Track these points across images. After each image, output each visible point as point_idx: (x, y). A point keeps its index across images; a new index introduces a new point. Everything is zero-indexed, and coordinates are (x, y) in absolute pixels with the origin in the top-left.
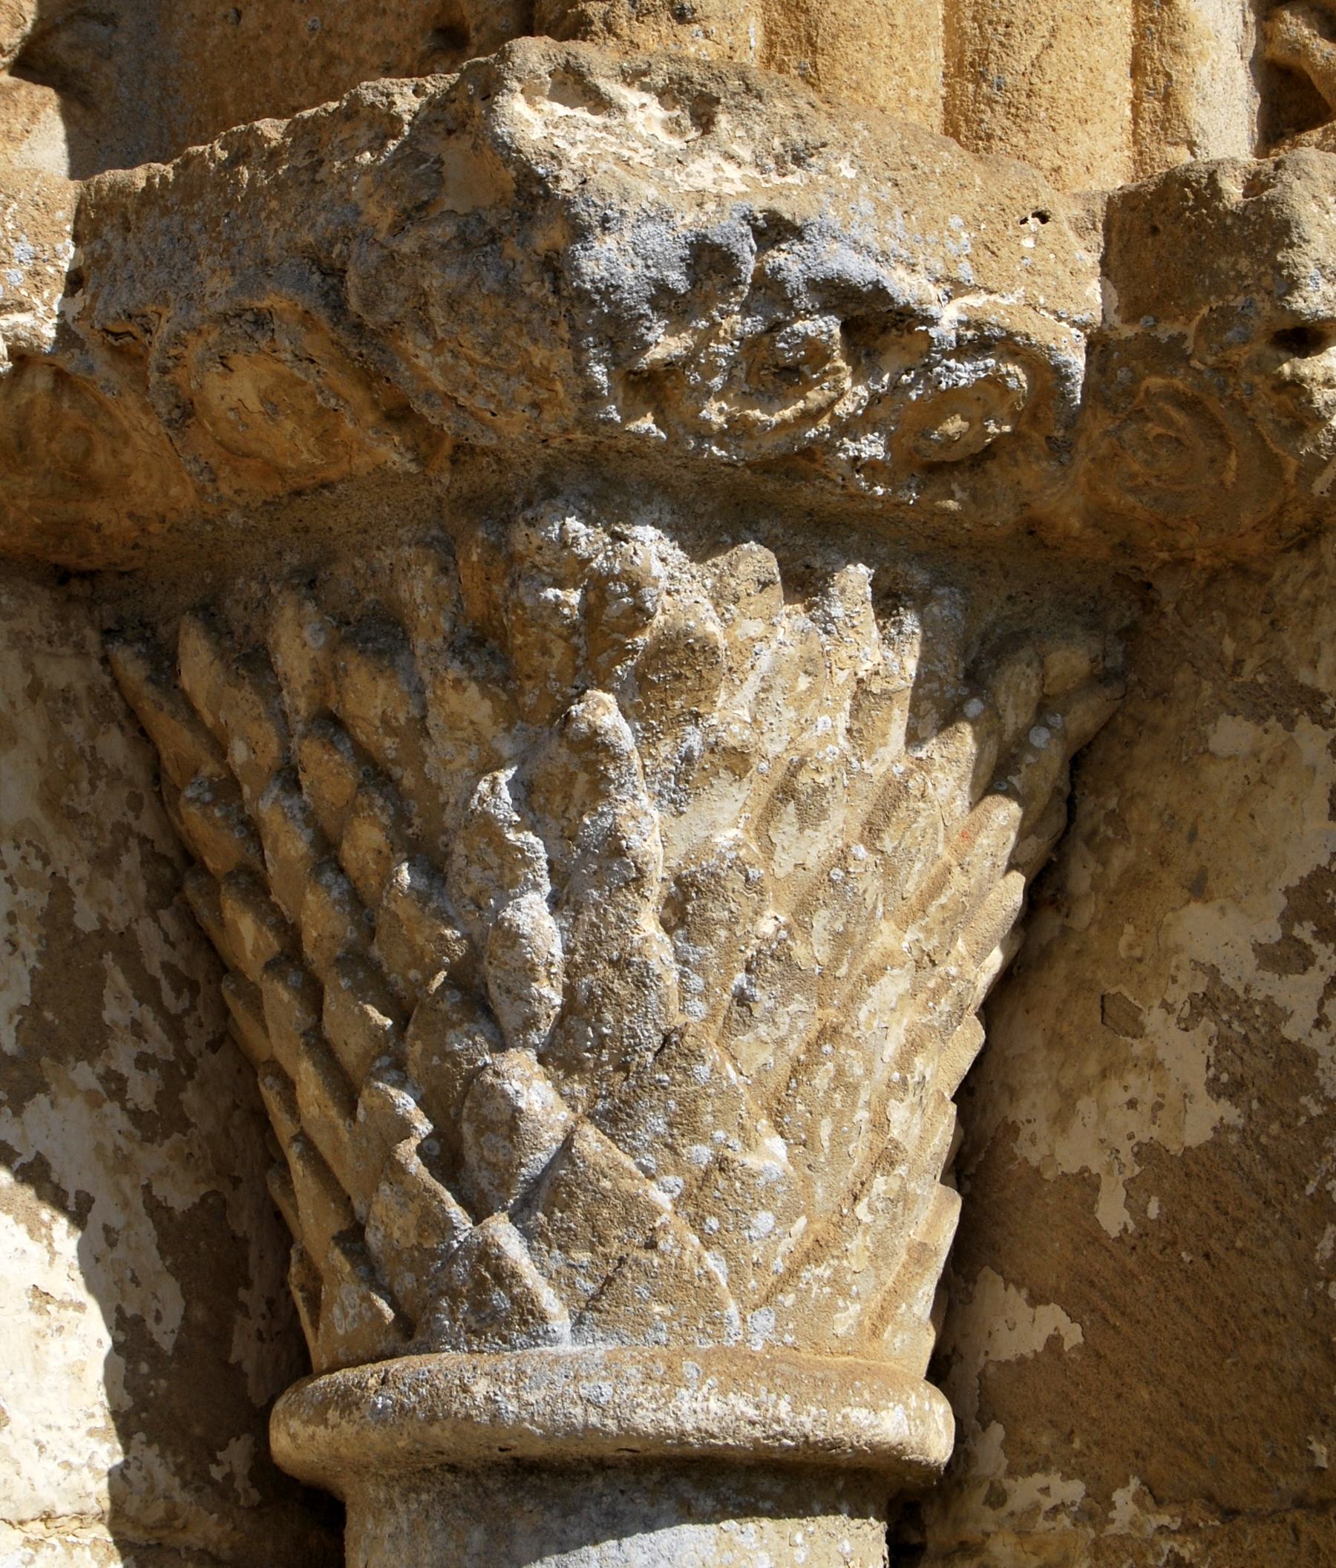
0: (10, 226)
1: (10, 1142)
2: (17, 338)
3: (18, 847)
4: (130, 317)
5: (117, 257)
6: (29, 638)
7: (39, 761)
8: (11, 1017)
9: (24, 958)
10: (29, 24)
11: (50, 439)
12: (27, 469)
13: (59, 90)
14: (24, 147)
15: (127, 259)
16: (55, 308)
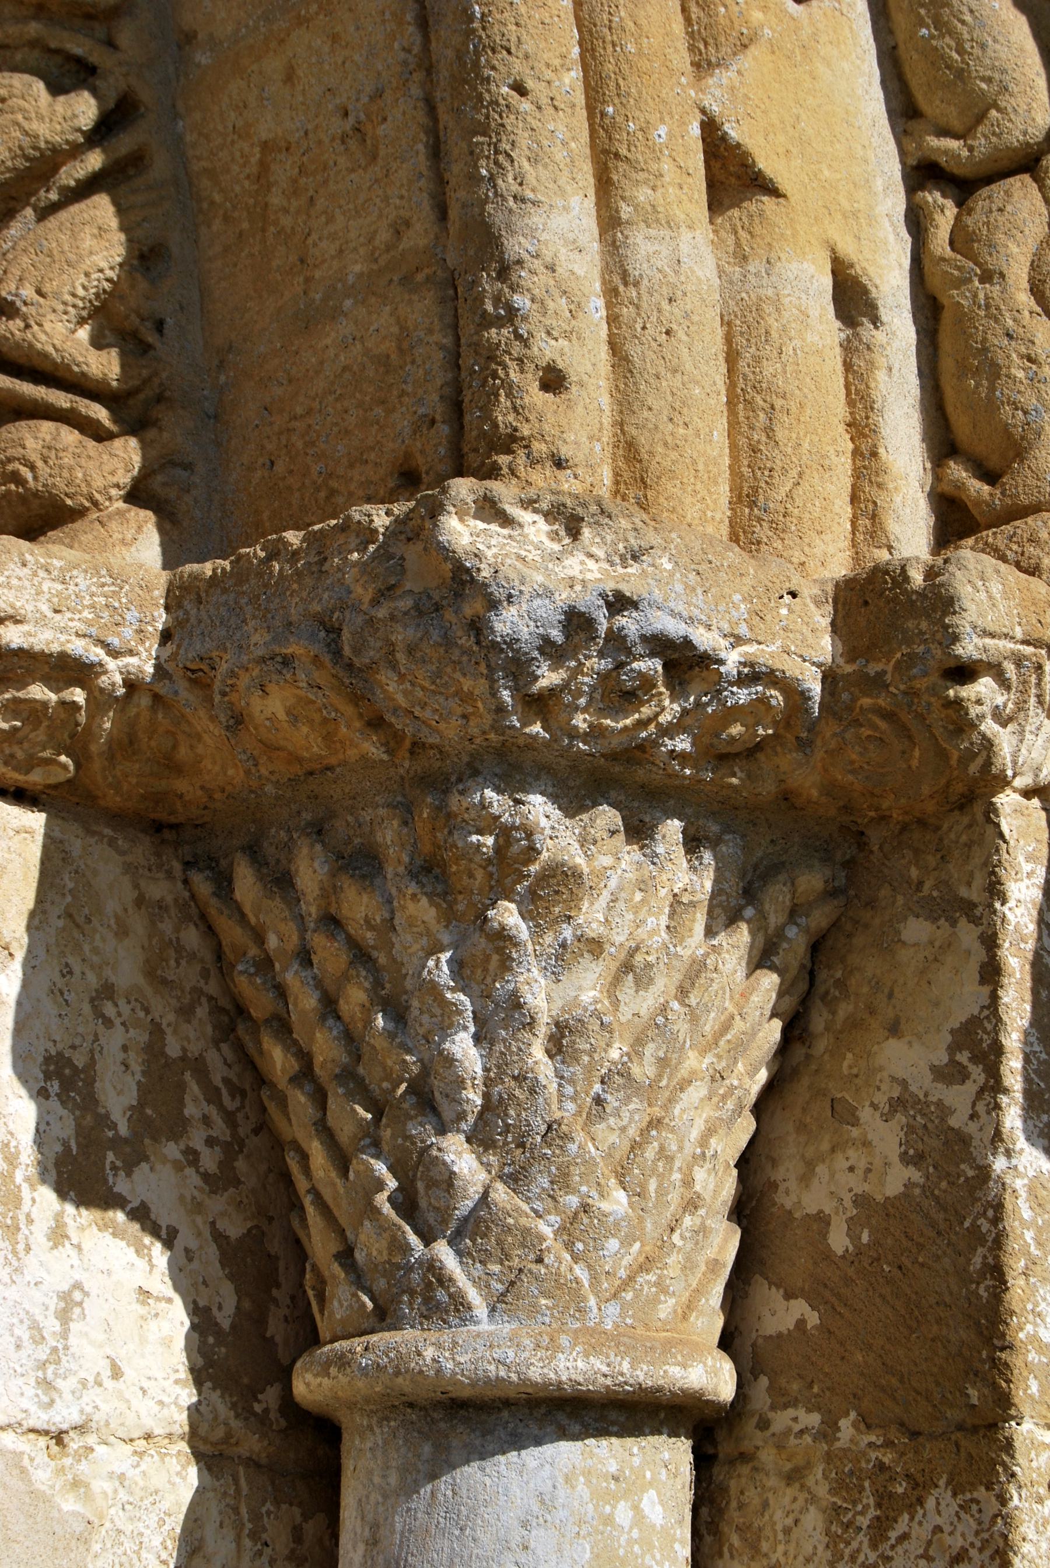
0: (124, 600)
2: (129, 673)
3: (129, 1002)
5: (193, 620)
7: (143, 947)
11: (150, 739)
13: (155, 512)
14: (133, 549)
15: (200, 622)
16: (154, 653)
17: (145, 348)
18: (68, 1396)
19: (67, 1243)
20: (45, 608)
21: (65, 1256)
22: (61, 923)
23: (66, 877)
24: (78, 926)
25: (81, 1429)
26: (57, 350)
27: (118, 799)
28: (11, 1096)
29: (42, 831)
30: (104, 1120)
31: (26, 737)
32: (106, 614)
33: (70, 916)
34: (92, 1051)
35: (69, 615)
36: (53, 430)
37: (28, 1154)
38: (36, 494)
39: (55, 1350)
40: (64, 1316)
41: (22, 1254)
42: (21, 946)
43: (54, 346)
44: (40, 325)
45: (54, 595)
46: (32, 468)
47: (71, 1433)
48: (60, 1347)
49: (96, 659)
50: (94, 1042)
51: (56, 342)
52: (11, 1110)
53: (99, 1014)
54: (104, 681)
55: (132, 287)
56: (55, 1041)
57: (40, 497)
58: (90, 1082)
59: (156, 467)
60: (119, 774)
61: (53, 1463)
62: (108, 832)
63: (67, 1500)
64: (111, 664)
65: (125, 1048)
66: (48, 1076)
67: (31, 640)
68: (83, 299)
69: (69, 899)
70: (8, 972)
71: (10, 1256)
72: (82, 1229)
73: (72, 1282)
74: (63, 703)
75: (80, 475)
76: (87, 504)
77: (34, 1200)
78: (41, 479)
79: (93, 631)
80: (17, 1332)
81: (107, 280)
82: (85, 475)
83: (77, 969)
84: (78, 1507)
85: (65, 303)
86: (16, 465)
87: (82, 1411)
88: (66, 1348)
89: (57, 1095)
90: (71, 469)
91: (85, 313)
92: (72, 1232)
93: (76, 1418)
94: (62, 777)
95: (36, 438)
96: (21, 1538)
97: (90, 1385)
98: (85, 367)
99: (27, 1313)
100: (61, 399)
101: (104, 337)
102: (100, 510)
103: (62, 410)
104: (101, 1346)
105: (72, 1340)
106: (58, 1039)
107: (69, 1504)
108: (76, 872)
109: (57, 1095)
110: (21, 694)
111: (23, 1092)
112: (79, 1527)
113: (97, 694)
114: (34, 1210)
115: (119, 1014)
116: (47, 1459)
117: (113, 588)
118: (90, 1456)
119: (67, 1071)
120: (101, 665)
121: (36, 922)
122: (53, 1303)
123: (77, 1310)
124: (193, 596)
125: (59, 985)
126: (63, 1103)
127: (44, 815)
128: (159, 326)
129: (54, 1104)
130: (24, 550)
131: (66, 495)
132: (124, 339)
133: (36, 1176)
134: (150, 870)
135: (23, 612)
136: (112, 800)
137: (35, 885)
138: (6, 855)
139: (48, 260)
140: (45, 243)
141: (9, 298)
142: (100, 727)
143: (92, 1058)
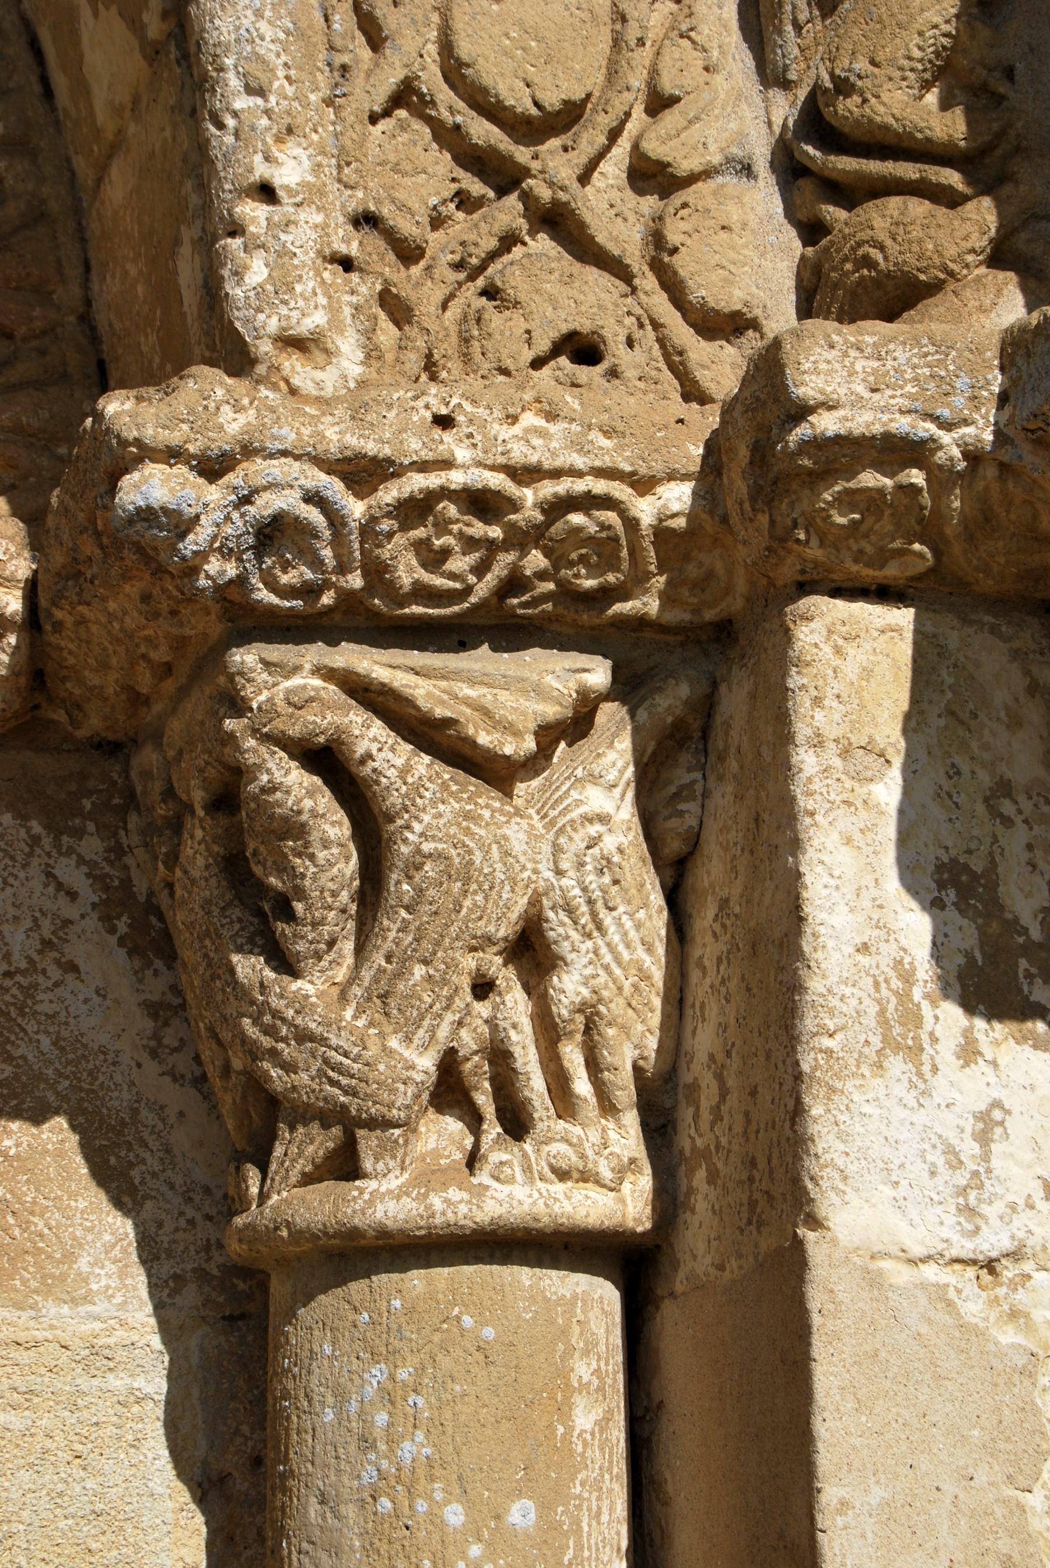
0: (951, 368)
1: (1043, 1002)
2: (966, 444)
3: (1030, 798)
4: (1035, 416)
5: (1025, 377)
6: (1026, 653)
7: (1041, 737)
8: (1036, 916)
9: (1042, 874)
10: (993, 230)
11: (1008, 512)
12: (997, 534)
13: (1017, 272)
14: (993, 315)
15: (1031, 376)
16: (992, 419)
17: (999, 99)
18: (994, 1222)
19: (980, 1060)
20: (861, 389)
21: (979, 1074)
22: (942, 722)
23: (944, 673)
24: (961, 722)
25: (1016, 1255)
26: (897, 120)
27: (991, 582)
28: (900, 910)
29: (911, 627)
30: (1014, 926)
31: (872, 529)
32: (932, 385)
33: (953, 713)
34: (991, 854)
35: (889, 392)
36: (901, 205)
37: (924, 969)
38: (888, 275)
39: (975, 1174)
40: (984, 1138)
41: (928, 1075)
42: (898, 751)
43: (893, 116)
44: (878, 97)
45: (869, 374)
46: (882, 248)
47: (1004, 1261)
48: (982, 1170)
49: (926, 435)
50: (992, 844)
51: (895, 111)
52: (902, 925)
53: (995, 813)
54: (940, 457)
55: (972, 37)
56: (946, 848)
57: (894, 277)
58: (993, 886)
59: (1016, 224)
60: (984, 555)
61: (984, 1294)
62: (988, 619)
63: (1005, 1333)
64: (946, 438)
65: (1030, 847)
66: (941, 885)
67: (848, 424)
68: (921, 60)
69: (949, 695)
70: (886, 780)
71: (914, 1079)
72: (997, 1043)
73: (990, 1100)
74: (900, 487)
75: (930, 247)
76: (942, 276)
77: (936, 1018)
78: (891, 258)
79: (918, 405)
80: (930, 1158)
81: (945, 35)
82: (935, 246)
83: (965, 769)
84: (1020, 1339)
85: (901, 69)
86: (866, 249)
87: (1013, 1237)
88: (989, 1171)
89: (954, 904)
90: (920, 242)
91: (927, 76)
92: (984, 1046)
93: (1006, 1244)
94: (921, 567)
95: (884, 216)
96: (954, 1375)
97: (1019, 1209)
98: (928, 132)
99: (940, 1137)
100: (908, 171)
101: (954, 97)
102: (958, 280)
103: (911, 182)
104: (1029, 1166)
105: (995, 1163)
106: (950, 844)
107: (1008, 1336)
108: (955, 666)
109: (954, 904)
110: (852, 485)
111: (914, 904)
112: (1021, 1361)
113: (936, 472)
114: (938, 1027)
115: (1020, 812)
116: (977, 1290)
117: (937, 357)
118: (1028, 1284)
119: (964, 878)
120: (934, 441)
121: (913, 723)
122: (969, 1125)
123: (998, 1131)
124: (1022, 351)
125: (946, 788)
126: (961, 911)
127: (912, 610)
128: (1009, 73)
129: (951, 913)
130: (830, 330)
131: (918, 270)
132: (975, 95)
133: (938, 992)
134: (1042, 654)
135: (835, 396)
136: (987, 585)
137: (908, 685)
138: (872, 658)
139: (878, 26)
140: (874, 9)
141: (843, 75)
142: (949, 507)
143: (993, 862)
